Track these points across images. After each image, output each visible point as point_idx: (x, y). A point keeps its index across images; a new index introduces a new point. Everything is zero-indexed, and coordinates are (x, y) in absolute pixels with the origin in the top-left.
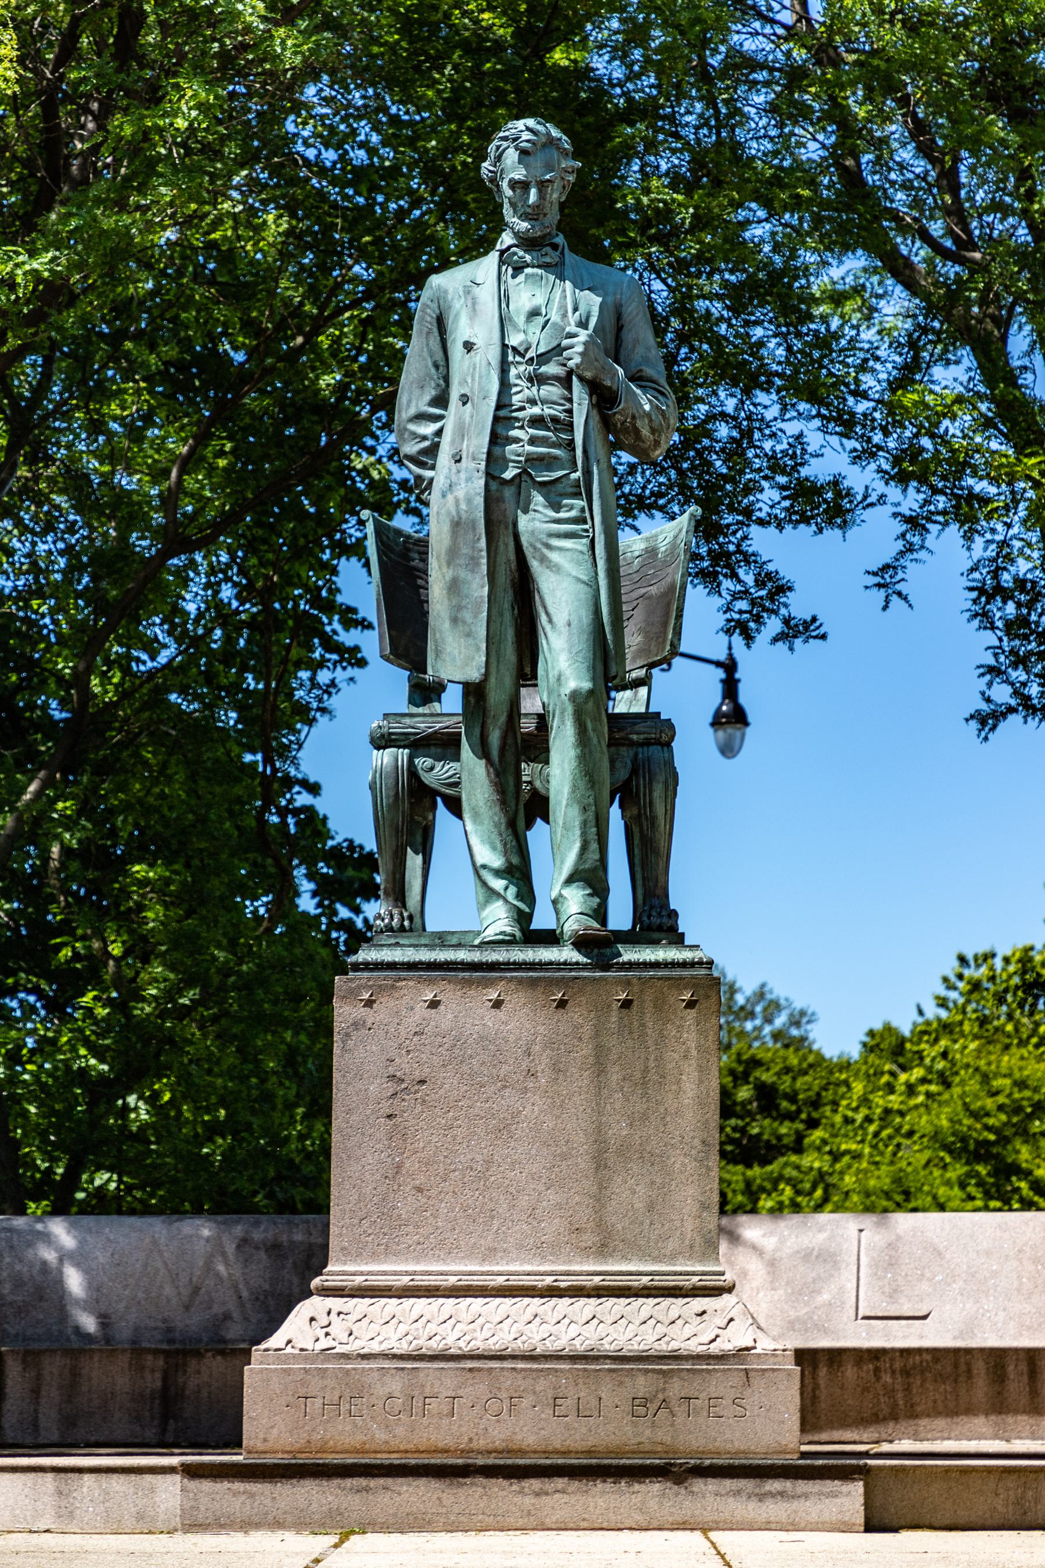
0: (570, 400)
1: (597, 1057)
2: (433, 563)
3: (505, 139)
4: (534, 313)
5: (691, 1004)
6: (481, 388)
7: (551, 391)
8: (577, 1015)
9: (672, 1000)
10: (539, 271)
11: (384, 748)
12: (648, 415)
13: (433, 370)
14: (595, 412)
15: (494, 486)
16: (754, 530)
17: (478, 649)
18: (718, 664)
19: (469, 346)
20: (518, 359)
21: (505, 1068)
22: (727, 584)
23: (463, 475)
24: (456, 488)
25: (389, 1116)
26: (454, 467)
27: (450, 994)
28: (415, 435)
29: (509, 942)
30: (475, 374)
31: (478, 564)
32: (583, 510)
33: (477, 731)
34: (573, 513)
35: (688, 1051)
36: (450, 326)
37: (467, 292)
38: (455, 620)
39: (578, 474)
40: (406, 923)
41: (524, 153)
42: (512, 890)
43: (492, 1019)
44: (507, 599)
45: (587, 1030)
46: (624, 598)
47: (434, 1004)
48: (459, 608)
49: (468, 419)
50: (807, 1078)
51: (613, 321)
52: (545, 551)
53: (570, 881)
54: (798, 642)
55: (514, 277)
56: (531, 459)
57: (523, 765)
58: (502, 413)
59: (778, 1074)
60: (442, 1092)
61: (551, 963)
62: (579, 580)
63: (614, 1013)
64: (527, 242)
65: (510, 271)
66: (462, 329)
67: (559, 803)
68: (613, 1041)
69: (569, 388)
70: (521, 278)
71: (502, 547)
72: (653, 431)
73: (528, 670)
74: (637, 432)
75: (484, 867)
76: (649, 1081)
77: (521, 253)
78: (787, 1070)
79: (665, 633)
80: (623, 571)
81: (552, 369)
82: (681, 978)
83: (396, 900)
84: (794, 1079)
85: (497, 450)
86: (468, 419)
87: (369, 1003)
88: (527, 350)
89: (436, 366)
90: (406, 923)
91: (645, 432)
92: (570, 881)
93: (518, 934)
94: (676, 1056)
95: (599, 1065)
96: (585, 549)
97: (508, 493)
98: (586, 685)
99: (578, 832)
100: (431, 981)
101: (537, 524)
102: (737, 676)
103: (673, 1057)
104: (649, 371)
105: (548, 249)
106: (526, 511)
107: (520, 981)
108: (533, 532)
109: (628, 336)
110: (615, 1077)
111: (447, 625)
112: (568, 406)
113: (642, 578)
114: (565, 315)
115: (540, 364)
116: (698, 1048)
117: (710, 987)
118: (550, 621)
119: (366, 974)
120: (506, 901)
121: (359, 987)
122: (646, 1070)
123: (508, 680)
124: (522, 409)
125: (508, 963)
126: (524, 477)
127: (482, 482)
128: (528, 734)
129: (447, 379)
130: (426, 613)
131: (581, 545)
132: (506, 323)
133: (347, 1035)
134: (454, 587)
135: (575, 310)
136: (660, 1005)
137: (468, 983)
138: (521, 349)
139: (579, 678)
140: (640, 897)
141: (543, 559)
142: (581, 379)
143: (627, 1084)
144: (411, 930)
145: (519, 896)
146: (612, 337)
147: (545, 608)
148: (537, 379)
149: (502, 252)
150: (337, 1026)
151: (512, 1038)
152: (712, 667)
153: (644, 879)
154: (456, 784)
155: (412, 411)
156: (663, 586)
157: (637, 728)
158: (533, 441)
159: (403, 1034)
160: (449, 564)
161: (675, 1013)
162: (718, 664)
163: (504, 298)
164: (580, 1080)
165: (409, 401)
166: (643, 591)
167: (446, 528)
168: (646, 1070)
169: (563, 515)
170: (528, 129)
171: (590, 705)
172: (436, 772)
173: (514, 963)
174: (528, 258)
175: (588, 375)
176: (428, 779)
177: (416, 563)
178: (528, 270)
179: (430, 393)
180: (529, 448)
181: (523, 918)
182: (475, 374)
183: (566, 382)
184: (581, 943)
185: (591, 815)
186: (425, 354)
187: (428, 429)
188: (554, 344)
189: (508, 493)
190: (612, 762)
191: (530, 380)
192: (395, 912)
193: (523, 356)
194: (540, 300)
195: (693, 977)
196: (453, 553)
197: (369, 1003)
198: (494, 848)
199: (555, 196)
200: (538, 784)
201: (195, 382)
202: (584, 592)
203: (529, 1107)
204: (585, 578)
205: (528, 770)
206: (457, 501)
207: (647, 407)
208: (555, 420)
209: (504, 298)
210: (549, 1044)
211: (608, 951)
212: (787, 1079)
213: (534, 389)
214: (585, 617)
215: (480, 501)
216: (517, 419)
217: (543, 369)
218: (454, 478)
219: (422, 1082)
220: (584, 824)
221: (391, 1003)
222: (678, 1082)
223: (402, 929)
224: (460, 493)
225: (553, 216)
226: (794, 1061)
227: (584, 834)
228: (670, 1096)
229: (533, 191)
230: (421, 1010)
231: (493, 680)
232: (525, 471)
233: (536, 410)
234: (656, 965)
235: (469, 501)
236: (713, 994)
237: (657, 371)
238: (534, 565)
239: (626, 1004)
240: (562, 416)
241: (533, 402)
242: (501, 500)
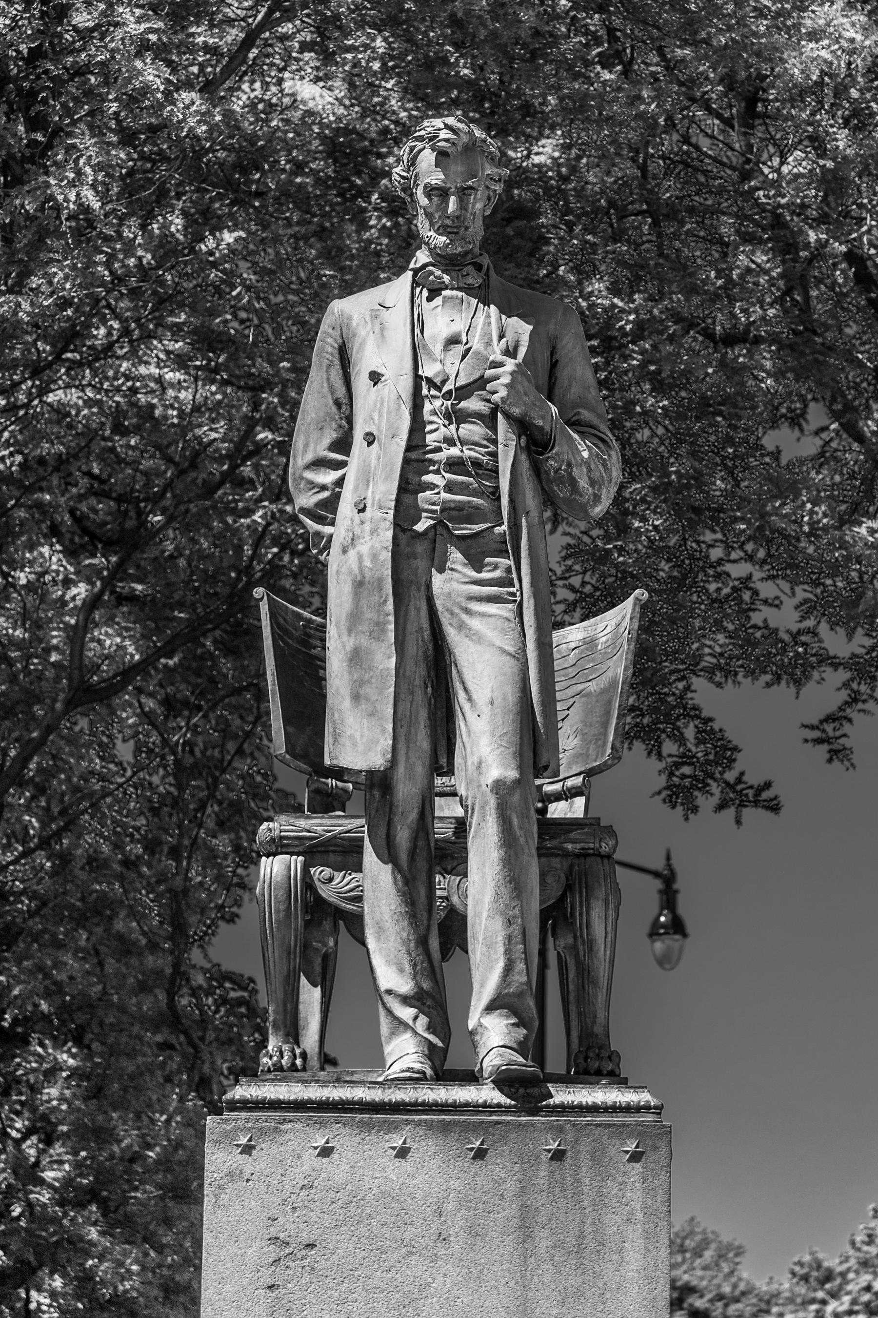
0: (495, 442)
1: (523, 1219)
2: (332, 631)
3: (421, 139)
4: (453, 341)
5: (635, 1157)
6: (390, 426)
7: (473, 430)
8: (500, 1168)
9: (612, 1151)
10: (460, 294)
11: (275, 855)
12: (587, 463)
13: (334, 409)
14: (523, 457)
15: (403, 538)
16: (698, 682)
17: (384, 730)
18: (656, 874)
19: (375, 377)
20: (433, 392)
21: (410, 1232)
22: (670, 747)
23: (367, 527)
24: (358, 545)
25: (270, 1287)
26: (357, 517)
27: (343, 1137)
28: (312, 485)
29: (417, 1079)
30: (381, 410)
31: (384, 631)
32: (509, 570)
33: (382, 831)
34: (497, 574)
35: (632, 1213)
36: (354, 356)
37: (375, 316)
38: (356, 698)
39: (504, 527)
40: (299, 1062)
41: (442, 155)
42: (423, 1020)
43: (396, 1172)
44: (418, 672)
45: (511, 1187)
46: (559, 696)
47: (326, 1152)
48: (361, 683)
49: (374, 462)
50: (739, 1306)
51: (547, 354)
52: (464, 617)
53: (490, 1008)
54: (748, 813)
55: (429, 299)
56: (446, 508)
57: (438, 877)
58: (413, 455)
59: (711, 1301)
60: (334, 1258)
61: (467, 1104)
62: (503, 651)
64: (447, 261)
65: (425, 293)
66: (368, 358)
67: (478, 915)
68: (543, 1199)
69: (494, 428)
70: (438, 301)
71: (413, 613)
72: (592, 483)
73: (443, 761)
74: (573, 482)
75: (389, 992)
76: (584, 1249)
77: (438, 273)
78: (720, 1297)
79: (605, 734)
80: (557, 665)
81: (473, 404)
82: (624, 1125)
83: (287, 1035)
84: (726, 1306)
85: (407, 499)
86: (374, 462)
87: (247, 1149)
88: (444, 382)
89: (338, 404)
90: (299, 1062)
91: (583, 483)
92: (490, 1008)
93: (429, 1072)
94: (617, 1219)
95: (525, 1232)
96: (511, 616)
97: (421, 548)
98: (512, 774)
99: (501, 950)
100: (323, 1124)
101: (455, 586)
102: (676, 886)
103: (613, 1220)
104: (586, 415)
105: (470, 268)
106: (441, 570)
107: (430, 1126)
108: (449, 595)
109: (563, 375)
110: (544, 1243)
111: (347, 703)
112: (492, 448)
113: (580, 673)
114: (489, 344)
115: (459, 399)
116: (645, 1209)
117: (659, 1136)
118: (470, 699)
119: (244, 1115)
120: (415, 1032)
121: (235, 1130)
122: (581, 1236)
123: (420, 769)
124: (438, 450)
125: (416, 1104)
126: (440, 529)
127: (390, 534)
128: (444, 841)
129: (350, 420)
130: (324, 697)
131: (504, 610)
132: (421, 352)
133: (221, 1187)
134: (356, 658)
135: (501, 336)
136: (596, 1158)
137: (368, 1127)
138: (438, 381)
139: (506, 766)
140: (575, 1034)
141: (461, 627)
142: (508, 416)
143: (558, 1253)
144: (304, 1069)
145: (430, 1028)
146: (544, 371)
147: (463, 683)
148: (456, 416)
149: (416, 272)
150: (209, 1176)
151: (419, 1194)
152: (649, 878)
153: (579, 1014)
154: (359, 899)
155: (310, 457)
156: (603, 682)
157: (572, 835)
158: (450, 488)
159: (288, 1187)
160: (350, 631)
161: (616, 1167)
162: (656, 874)
163: (417, 324)
164: (501, 1247)
165: (306, 445)
166: (580, 687)
167: (347, 588)
168: (581, 1236)
169: (485, 575)
170: (447, 127)
171: (516, 798)
172: (335, 885)
173: (423, 1104)
174: (446, 278)
175: (516, 411)
176: (325, 892)
177: (316, 652)
178: (446, 293)
179: (330, 435)
182: (381, 410)
183: (490, 420)
184: (504, 1081)
185: (516, 929)
186: (326, 390)
187: (328, 477)
188: (477, 375)
189: (421, 548)
190: (543, 875)
191: (448, 416)
192: (285, 1047)
193: (439, 389)
194: (459, 326)
195: (638, 1124)
196: (354, 619)
197: (247, 1149)
198: (401, 971)
199: (479, 206)
200: (455, 899)
201: (111, 537)
202: (510, 666)
203: (440, 1278)
204: (511, 650)
205: (443, 883)
206: (360, 558)
207: (585, 454)
208: (476, 464)
209: (417, 324)
210: (464, 1202)
211: (536, 1091)
212: (720, 1304)
213: (453, 427)
214: (511, 695)
215: (386, 556)
216: (432, 462)
217: (463, 404)
218: (357, 531)
219: (311, 1246)
220: (509, 938)
221: (275, 1150)
222: (621, 1251)
224: (364, 548)
225: (476, 230)
226: (727, 1289)
227: (508, 952)
228: (611, 1268)
229: (452, 199)
230: (310, 1159)
231: (401, 769)
232: (440, 523)
233: (455, 451)
234: (594, 1109)
235: (374, 557)
236: (663, 1144)
237: (596, 413)
238: (451, 633)
239: (558, 1156)
240: (485, 459)
241: (450, 442)
242: (415, 550)
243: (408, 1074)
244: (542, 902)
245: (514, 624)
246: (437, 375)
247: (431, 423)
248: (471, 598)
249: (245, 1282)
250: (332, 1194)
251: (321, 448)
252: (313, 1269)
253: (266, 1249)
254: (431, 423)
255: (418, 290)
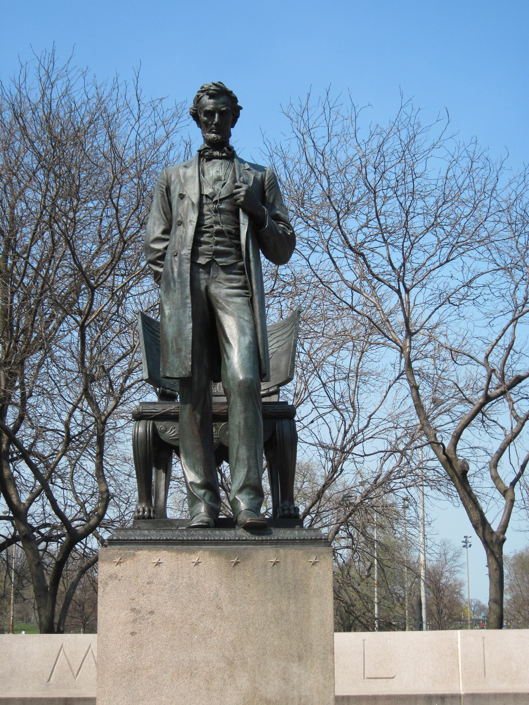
4: (219, 179)
20: (209, 201)
32: (246, 282)
53: (240, 491)
63: (269, 570)
88: (213, 197)
92: (240, 491)
100: (251, 330)
133: (106, 584)
179: (162, 228)
180: (214, 247)
181: (213, 511)
187: (159, 246)
208: (229, 232)
209: (202, 173)
219: (152, 613)
223: (149, 517)
230: (151, 569)
241: (217, 223)
243: (201, 524)
244: (264, 439)
245: (247, 308)
246: (210, 194)
247: (208, 215)
248: (229, 295)
249: (119, 631)
250: (162, 586)
251: (158, 232)
252: (153, 624)
253: (129, 614)
254: (208, 215)
255: (202, 159)
